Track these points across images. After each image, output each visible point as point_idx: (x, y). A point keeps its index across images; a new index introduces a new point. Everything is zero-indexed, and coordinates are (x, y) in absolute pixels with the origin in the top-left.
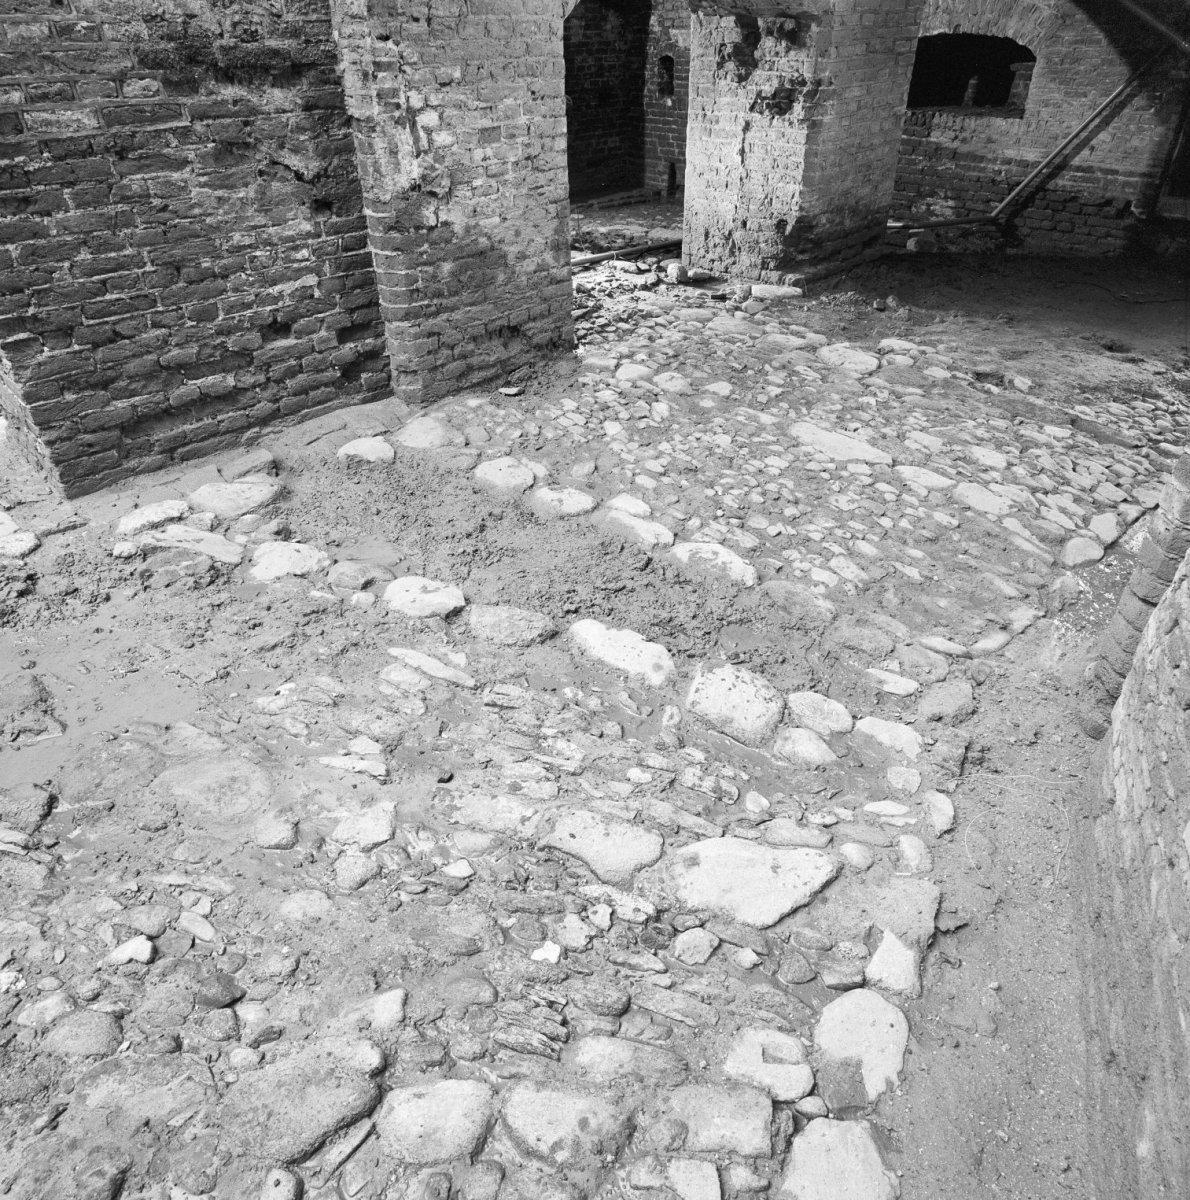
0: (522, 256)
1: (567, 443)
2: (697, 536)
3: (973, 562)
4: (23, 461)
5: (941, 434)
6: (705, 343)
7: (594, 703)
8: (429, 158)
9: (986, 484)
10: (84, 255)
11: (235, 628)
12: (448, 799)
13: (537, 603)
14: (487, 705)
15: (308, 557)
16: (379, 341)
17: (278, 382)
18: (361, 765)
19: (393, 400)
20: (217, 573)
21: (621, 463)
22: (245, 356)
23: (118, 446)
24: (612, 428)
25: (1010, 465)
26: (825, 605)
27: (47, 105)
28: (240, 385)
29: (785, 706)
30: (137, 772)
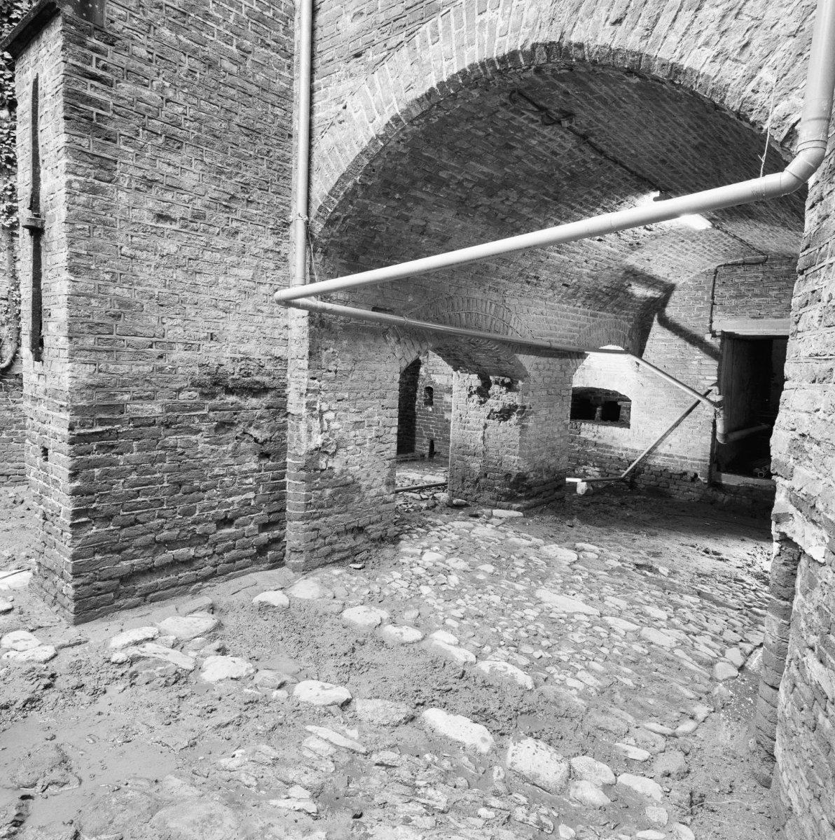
0: (370, 488)
1: (398, 598)
2: (490, 657)
3: (662, 676)
4: (39, 600)
5: (625, 599)
6: (473, 541)
7: (446, 764)
8: (327, 434)
9: (659, 628)
10: (134, 476)
11: (198, 712)
12: (363, 828)
13: (398, 698)
14: (377, 764)
15: (240, 666)
16: (282, 532)
17: (219, 554)
18: (299, 806)
19: (285, 569)
20: (179, 677)
21: (435, 611)
22: (205, 536)
23: (114, 591)
24: (425, 590)
25: (669, 618)
26: (580, 702)
27: (140, 401)
28: (197, 555)
29: (570, 767)
30: (139, 813)
